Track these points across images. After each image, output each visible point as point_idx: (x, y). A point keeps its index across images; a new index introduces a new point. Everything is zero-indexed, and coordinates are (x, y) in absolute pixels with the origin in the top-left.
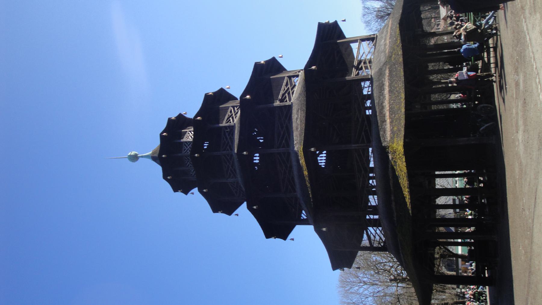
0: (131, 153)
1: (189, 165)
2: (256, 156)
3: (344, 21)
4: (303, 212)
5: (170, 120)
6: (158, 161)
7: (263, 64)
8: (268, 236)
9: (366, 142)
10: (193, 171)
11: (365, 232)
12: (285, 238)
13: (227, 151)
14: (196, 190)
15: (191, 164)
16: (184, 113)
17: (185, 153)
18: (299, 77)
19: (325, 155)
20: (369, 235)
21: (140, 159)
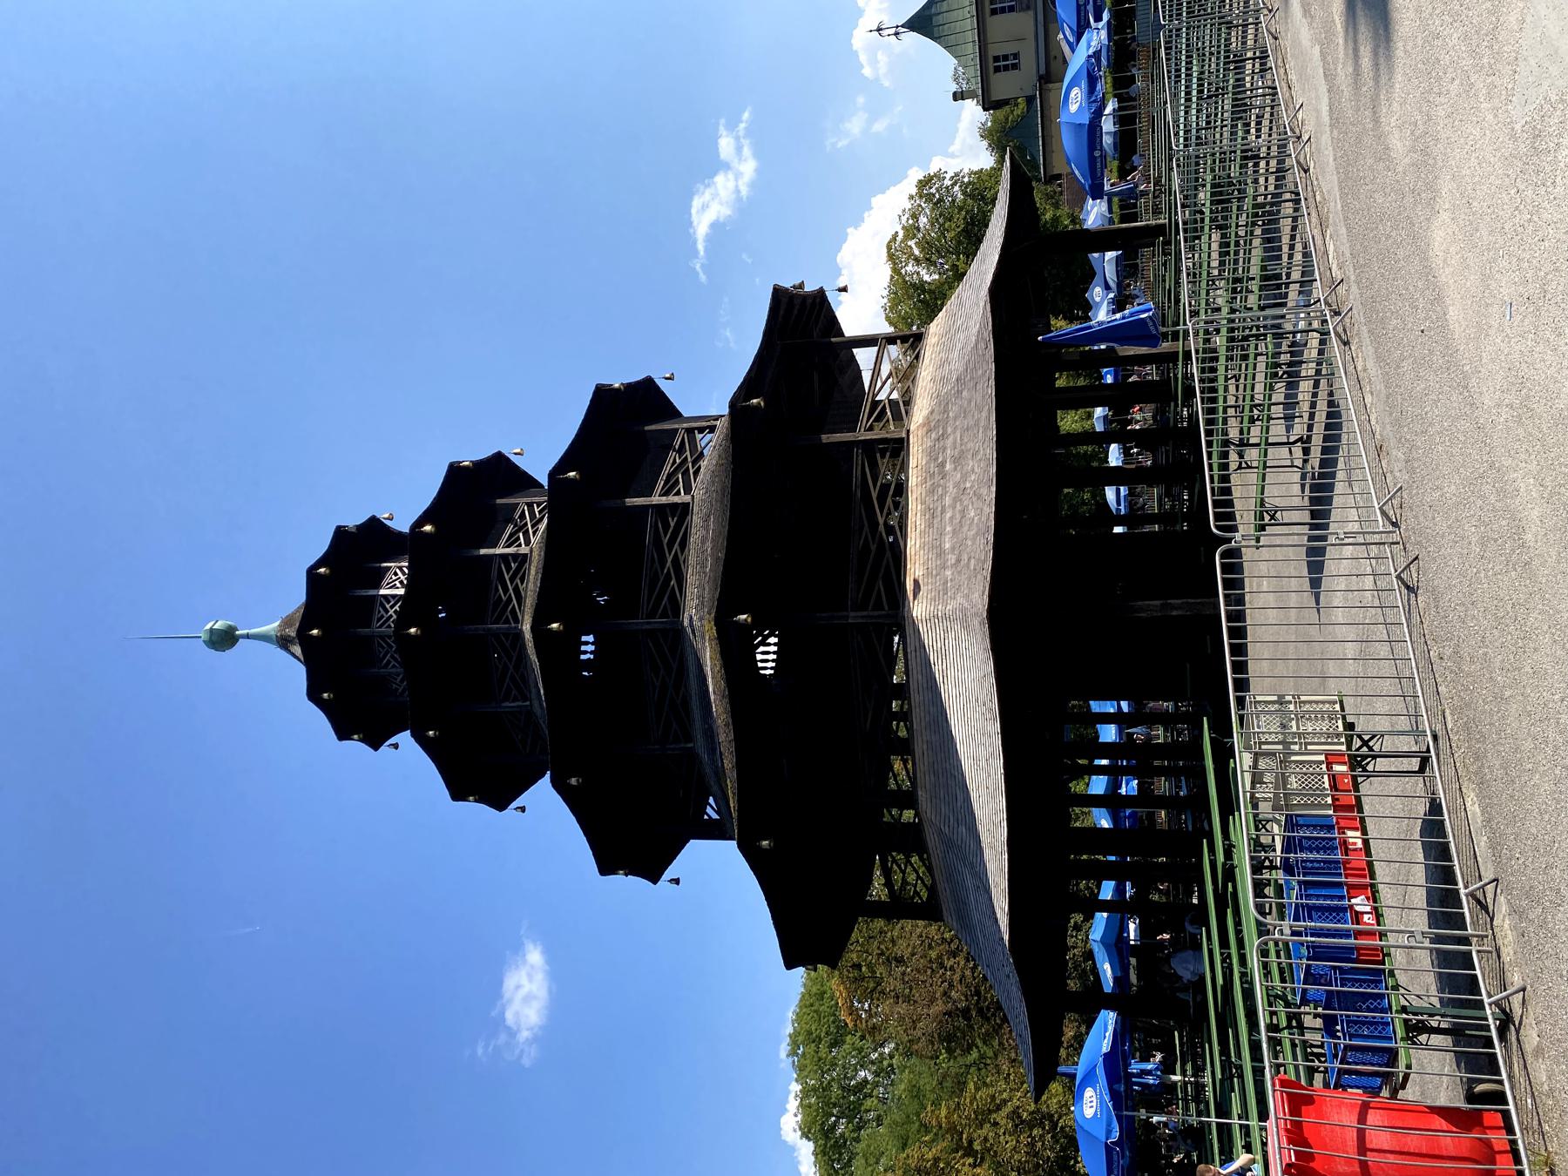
0: (213, 625)
1: (389, 662)
2: (587, 643)
4: (711, 800)
5: (340, 533)
7: (618, 390)
8: (606, 868)
9: (886, 608)
10: (402, 681)
12: (654, 878)
14: (405, 738)
15: (395, 660)
16: (386, 516)
17: (381, 626)
18: (717, 432)
19: (775, 649)
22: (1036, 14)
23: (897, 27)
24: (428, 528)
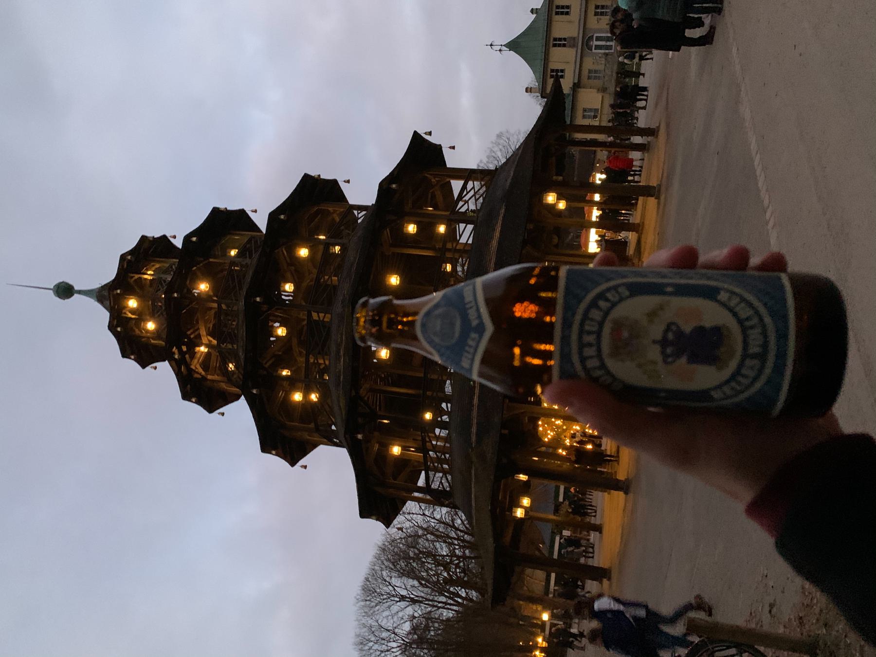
3: (453, 148)
12: (293, 463)
21: (76, 295)
22: (577, 51)
23: (501, 45)
24: (194, 239)
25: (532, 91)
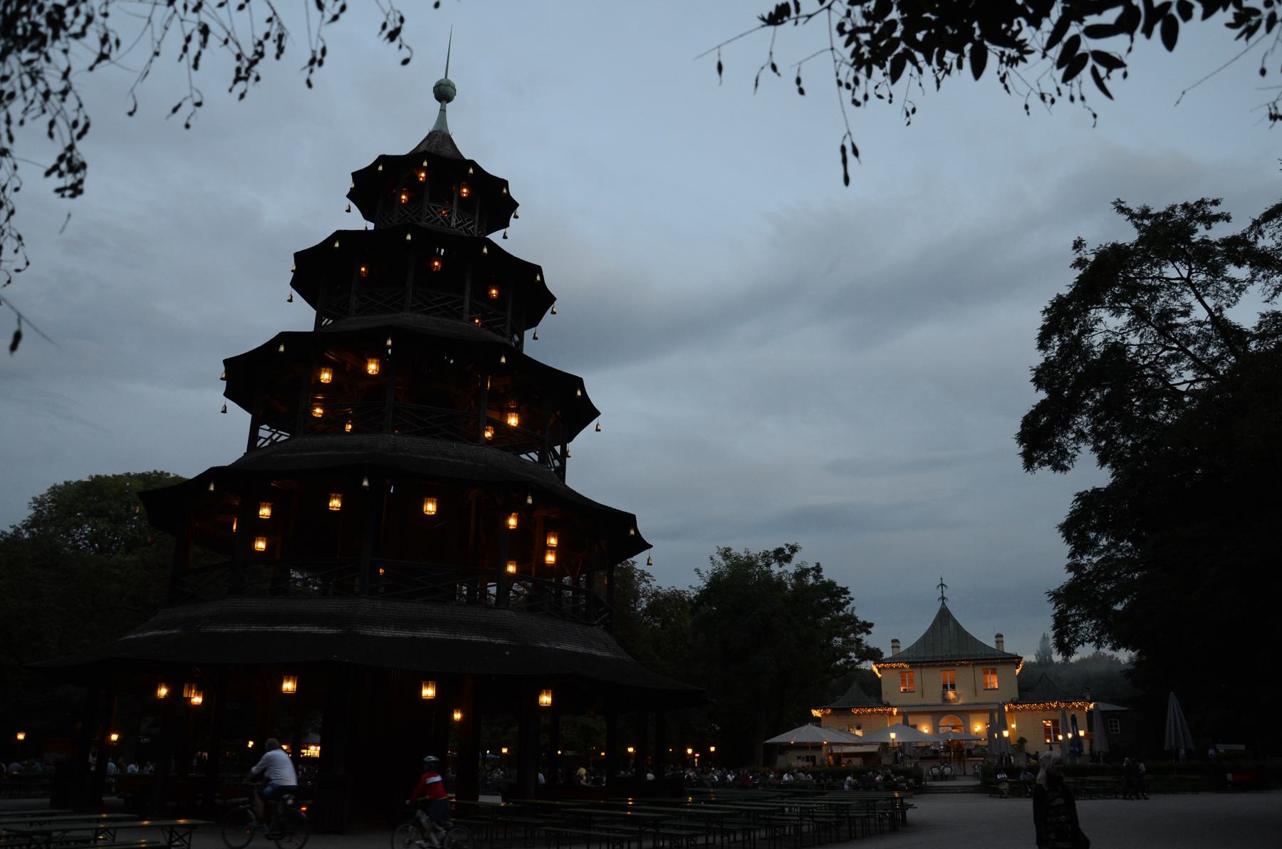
6: (422, 149)
11: (278, 441)
13: (412, 300)
20: (287, 439)
25: (895, 649)
